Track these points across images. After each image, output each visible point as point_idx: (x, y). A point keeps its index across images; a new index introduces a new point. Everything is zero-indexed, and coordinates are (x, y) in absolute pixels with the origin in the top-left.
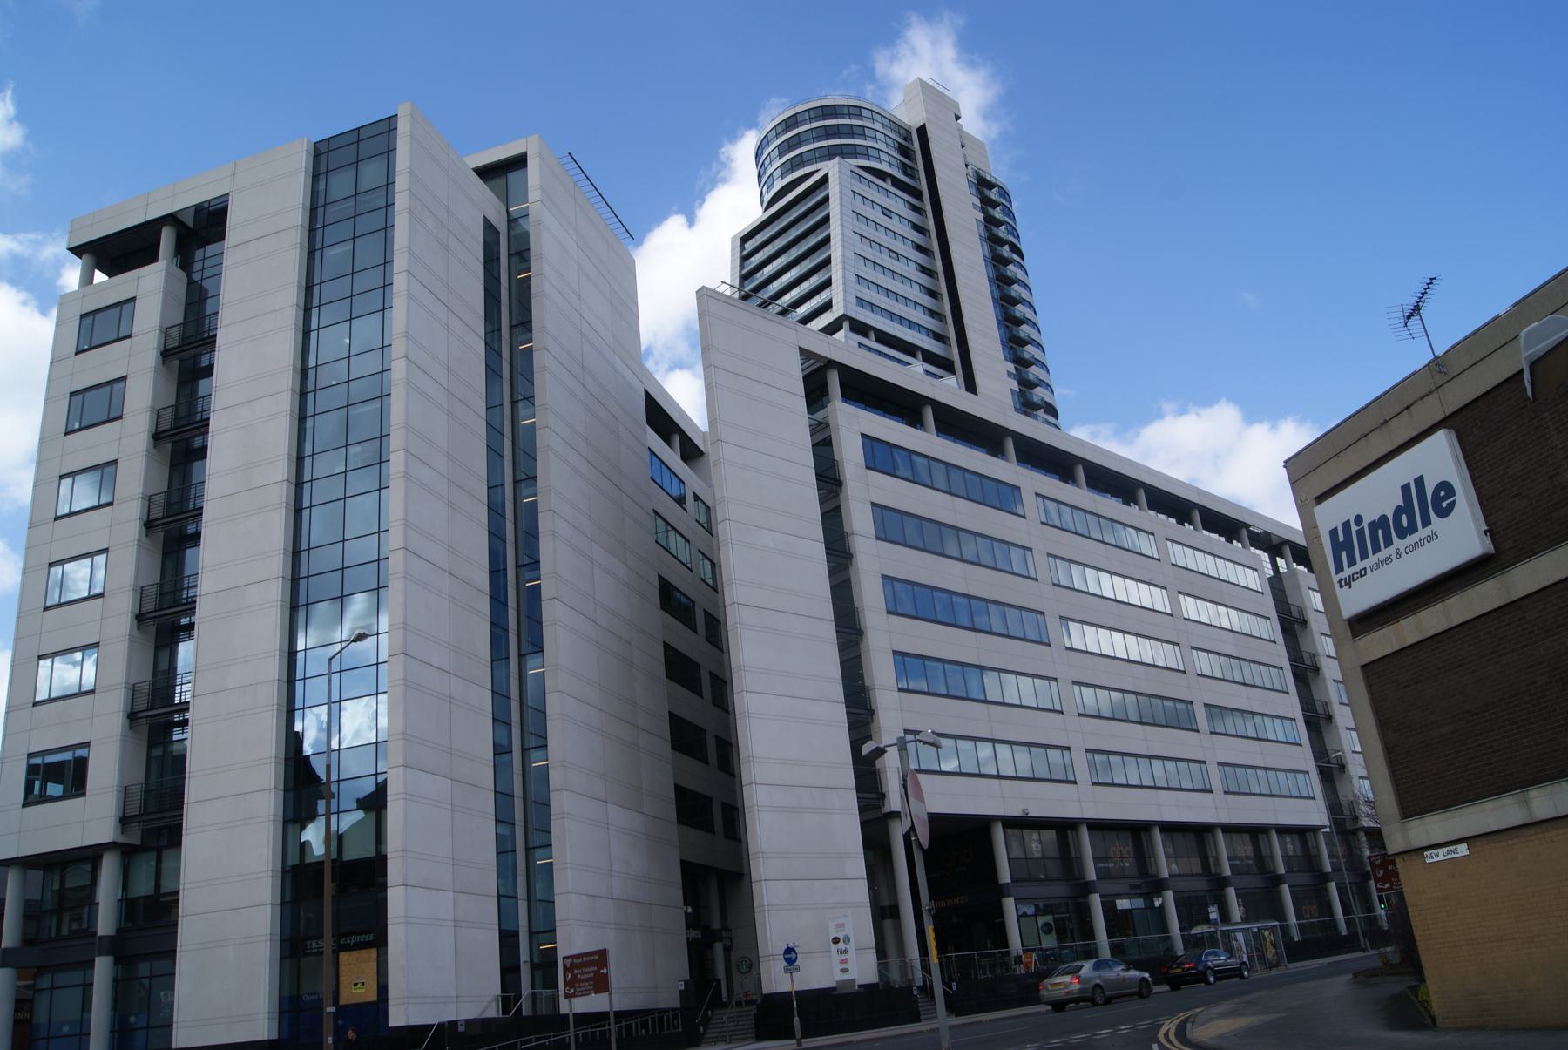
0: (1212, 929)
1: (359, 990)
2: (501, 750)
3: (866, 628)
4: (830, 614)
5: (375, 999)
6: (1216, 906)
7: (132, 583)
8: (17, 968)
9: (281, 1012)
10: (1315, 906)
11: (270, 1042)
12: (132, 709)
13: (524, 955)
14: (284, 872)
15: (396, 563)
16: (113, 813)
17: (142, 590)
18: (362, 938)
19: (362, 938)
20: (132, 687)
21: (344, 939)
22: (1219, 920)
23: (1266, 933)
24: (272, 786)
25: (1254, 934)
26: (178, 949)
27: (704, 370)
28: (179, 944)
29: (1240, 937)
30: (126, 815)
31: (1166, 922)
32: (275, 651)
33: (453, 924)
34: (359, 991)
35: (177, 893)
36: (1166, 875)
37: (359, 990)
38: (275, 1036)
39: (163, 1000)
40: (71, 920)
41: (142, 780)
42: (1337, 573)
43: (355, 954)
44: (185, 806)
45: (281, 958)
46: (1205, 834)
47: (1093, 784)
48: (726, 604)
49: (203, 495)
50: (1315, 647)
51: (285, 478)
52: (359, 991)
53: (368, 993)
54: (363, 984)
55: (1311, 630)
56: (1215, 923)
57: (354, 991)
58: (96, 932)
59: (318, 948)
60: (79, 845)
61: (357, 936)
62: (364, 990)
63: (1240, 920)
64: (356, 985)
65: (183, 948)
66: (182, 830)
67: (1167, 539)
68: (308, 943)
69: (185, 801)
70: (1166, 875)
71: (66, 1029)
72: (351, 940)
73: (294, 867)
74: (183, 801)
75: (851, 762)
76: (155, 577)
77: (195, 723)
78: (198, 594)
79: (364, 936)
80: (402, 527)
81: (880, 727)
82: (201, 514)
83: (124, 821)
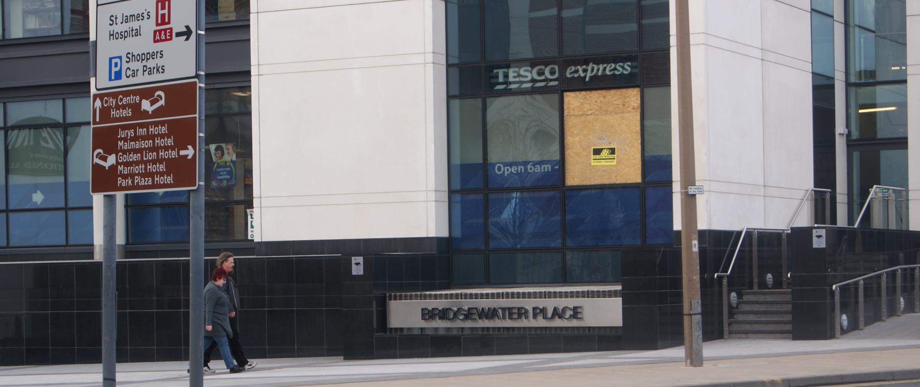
5: (638, 179)
11: (439, 240)
13: (840, 127)
18: (608, 69)
19: (608, 69)
21: (573, 68)
22: (388, 299)
31: (535, 285)
33: (758, 54)
38: (445, 233)
40: (26, 13)
42: (161, 10)
43: (595, 97)
45: (449, 97)
52: (603, 163)
54: (612, 151)
57: (594, 163)
58: (89, 39)
61: (598, 64)
62: (614, 163)
64: (597, 152)
65: (263, 70)
68: (501, 72)
71: (38, 198)
72: (585, 71)
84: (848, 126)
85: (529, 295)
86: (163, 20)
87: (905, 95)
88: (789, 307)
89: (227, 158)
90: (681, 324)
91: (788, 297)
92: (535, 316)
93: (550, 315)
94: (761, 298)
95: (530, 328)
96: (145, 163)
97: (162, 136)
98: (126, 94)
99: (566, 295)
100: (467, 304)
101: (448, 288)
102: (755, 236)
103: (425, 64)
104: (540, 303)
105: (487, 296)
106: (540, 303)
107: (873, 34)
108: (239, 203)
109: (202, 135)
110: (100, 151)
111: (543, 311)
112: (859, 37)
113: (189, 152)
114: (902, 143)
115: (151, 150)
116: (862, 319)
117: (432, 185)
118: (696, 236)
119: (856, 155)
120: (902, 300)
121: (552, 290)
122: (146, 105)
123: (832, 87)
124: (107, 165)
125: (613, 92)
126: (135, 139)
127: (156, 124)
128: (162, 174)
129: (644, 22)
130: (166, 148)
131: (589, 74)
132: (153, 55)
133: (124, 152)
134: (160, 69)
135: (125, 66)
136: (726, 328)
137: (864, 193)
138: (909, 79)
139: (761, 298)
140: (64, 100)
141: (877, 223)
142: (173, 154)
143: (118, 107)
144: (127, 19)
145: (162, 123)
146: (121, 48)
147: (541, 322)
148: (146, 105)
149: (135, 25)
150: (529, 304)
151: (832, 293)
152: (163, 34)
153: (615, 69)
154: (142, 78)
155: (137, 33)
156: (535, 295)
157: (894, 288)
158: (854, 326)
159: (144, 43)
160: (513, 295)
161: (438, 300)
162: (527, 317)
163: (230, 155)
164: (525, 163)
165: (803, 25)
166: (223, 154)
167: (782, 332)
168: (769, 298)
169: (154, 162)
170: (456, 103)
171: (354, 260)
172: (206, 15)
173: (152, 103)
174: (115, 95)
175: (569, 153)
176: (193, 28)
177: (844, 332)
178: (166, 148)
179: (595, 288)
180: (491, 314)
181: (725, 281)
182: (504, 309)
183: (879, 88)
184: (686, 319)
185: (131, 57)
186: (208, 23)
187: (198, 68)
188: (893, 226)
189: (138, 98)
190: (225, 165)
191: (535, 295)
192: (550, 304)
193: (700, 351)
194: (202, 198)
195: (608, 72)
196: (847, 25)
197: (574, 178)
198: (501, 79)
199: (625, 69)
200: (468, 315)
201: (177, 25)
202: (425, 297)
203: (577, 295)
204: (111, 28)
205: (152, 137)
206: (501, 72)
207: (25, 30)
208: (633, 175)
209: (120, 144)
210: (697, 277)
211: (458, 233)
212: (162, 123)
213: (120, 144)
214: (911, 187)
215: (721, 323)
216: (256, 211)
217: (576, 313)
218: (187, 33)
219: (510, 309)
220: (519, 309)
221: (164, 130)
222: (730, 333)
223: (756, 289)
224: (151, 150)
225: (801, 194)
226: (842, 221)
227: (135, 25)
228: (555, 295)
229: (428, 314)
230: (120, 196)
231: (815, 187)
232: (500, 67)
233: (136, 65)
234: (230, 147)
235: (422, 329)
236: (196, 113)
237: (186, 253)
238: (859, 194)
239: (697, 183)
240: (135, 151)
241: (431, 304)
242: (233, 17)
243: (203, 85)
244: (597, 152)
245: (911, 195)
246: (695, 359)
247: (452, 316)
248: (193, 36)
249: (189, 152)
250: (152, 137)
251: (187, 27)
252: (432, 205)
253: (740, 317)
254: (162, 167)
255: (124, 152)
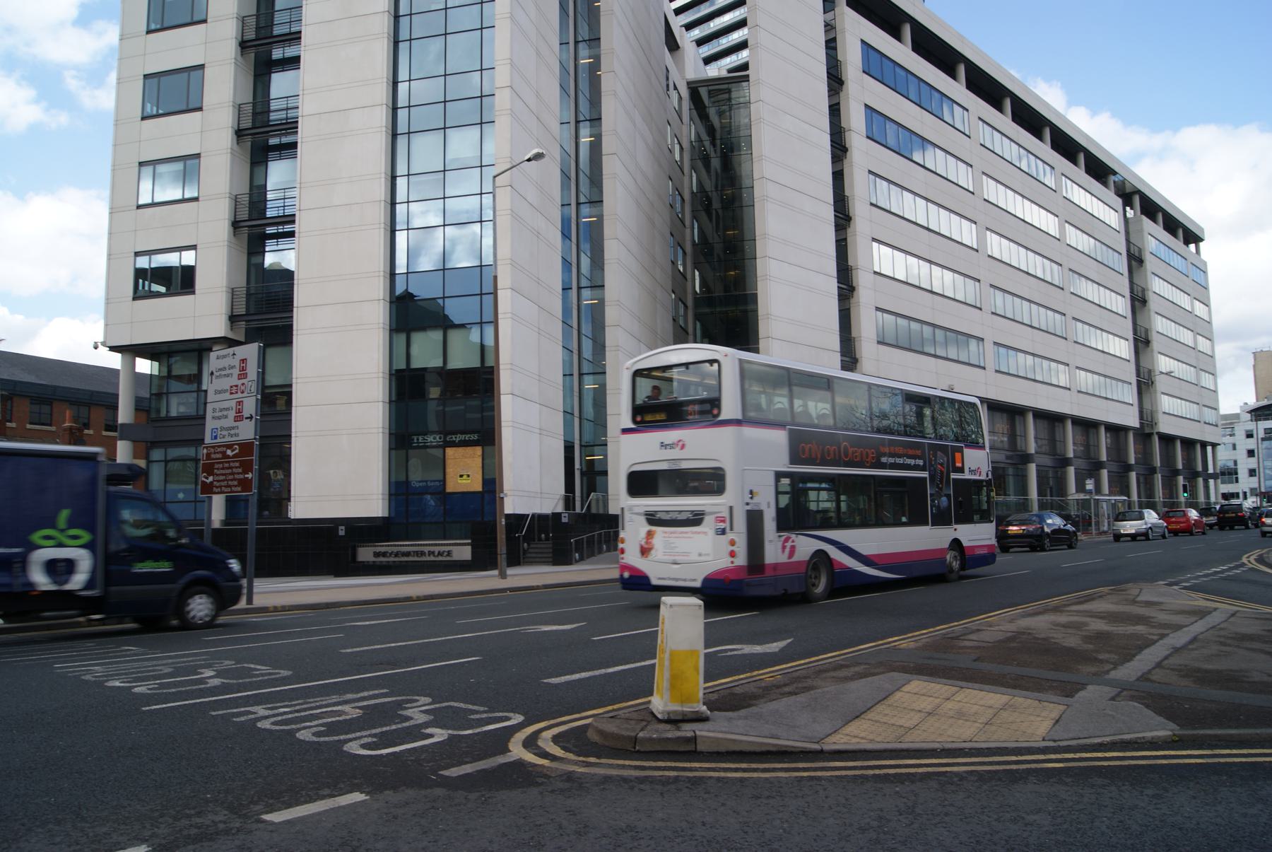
0: (1088, 497)
1: (464, 481)
2: (566, 289)
3: (855, 215)
4: (831, 201)
5: (481, 490)
6: (1093, 479)
7: (231, 100)
8: (134, 441)
9: (390, 495)
10: (1118, 489)
11: (383, 518)
12: (235, 218)
13: (577, 465)
14: (391, 375)
15: (502, 100)
16: (224, 311)
17: (240, 108)
18: (467, 437)
19: (467, 437)
20: (234, 198)
21: (450, 436)
23: (1120, 505)
24: (382, 298)
25: (1112, 504)
26: (293, 435)
27: (112, 212)
28: (293, 430)
29: (1104, 505)
30: (234, 314)
32: (381, 173)
33: (538, 431)
34: (464, 481)
35: (291, 386)
36: (1033, 451)
37: (464, 481)
38: (387, 515)
39: (272, 477)
40: (179, 404)
41: (244, 284)
43: (461, 450)
44: (295, 310)
45: (390, 449)
46: (1057, 424)
47: (997, 371)
48: (755, 178)
49: (301, 20)
50: (1146, 282)
51: (387, 10)
52: (464, 481)
53: (474, 483)
54: (468, 476)
55: (1146, 269)
56: (1090, 492)
57: (460, 482)
59: (425, 443)
60: (192, 338)
61: (462, 434)
62: (469, 481)
63: (1107, 493)
64: (461, 476)
66: (292, 330)
67: (1063, 174)
68: (415, 438)
69: (295, 305)
70: (1033, 451)
71: (181, 496)
72: (456, 438)
73: (398, 371)
74: (293, 305)
75: (838, 329)
76: (249, 98)
77: (301, 235)
78: (300, 114)
79: (469, 435)
80: (509, 66)
81: (859, 302)
82: (300, 38)
83: (233, 319)
84: (581, 465)
85: (426, 545)
86: (239, 411)
87: (606, 450)
88: (551, 550)
89: (279, 477)
90: (496, 558)
91: (551, 546)
92: (429, 555)
93: (436, 554)
94: (539, 546)
95: (427, 561)
96: (227, 480)
97: (237, 467)
98: (219, 446)
99: (444, 545)
100: (395, 549)
101: (388, 541)
102: (536, 516)
103: (378, 433)
104: (432, 549)
105: (406, 545)
106: (432, 549)
107: (592, 423)
108: (285, 499)
109: (257, 467)
110: (205, 474)
111: (433, 553)
112: (586, 425)
113: (250, 476)
114: (605, 473)
115: (230, 474)
116: (585, 555)
117: (380, 492)
118: (504, 517)
119: (585, 478)
120: (604, 546)
121: (437, 542)
122: (229, 452)
123: (573, 447)
124: (208, 481)
125: (469, 448)
126: (223, 469)
127: (234, 462)
128: (236, 486)
129: (484, 414)
130: (238, 473)
131: (458, 439)
132: (233, 428)
133: (217, 475)
134: (237, 435)
135: (219, 432)
136: (522, 561)
137: (588, 496)
138: (608, 444)
139: (539, 546)
140: (196, 447)
141: (594, 511)
142: (241, 476)
143: (215, 453)
144: (221, 410)
145: (237, 461)
146: (218, 424)
147: (432, 558)
148: (229, 452)
149: (225, 413)
150: (426, 549)
151: (571, 543)
152: (239, 417)
153: (452, 438)
154: (228, 439)
155: (226, 417)
156: (429, 545)
157: (601, 541)
158: (582, 559)
159: (229, 422)
160: (419, 545)
161: (383, 547)
162: (425, 556)
163: (280, 476)
164: (426, 481)
165: (560, 418)
166: (277, 475)
167: (548, 562)
168: (543, 546)
169: (232, 480)
170: (393, 452)
171: (340, 528)
172: (117, 396)
173: (232, 451)
174: (213, 447)
175: (448, 477)
176: (254, 415)
177: (577, 562)
178: (238, 473)
179: (458, 542)
180: (407, 554)
181: (521, 538)
182: (414, 552)
183: (596, 448)
184: (499, 556)
185: (222, 429)
186: (264, 414)
187: (256, 434)
188: (601, 511)
189: (225, 449)
190: (278, 480)
191: (429, 545)
192: (436, 549)
193: (506, 572)
194: (256, 497)
195: (467, 439)
196: (580, 418)
197: (450, 488)
198: (415, 441)
199: (475, 437)
200: (397, 555)
201: (246, 414)
202: (375, 546)
203: (450, 545)
204: (213, 414)
205: (231, 468)
206: (415, 438)
207: (178, 413)
208: (478, 487)
209: (215, 471)
210: (504, 536)
211: (393, 515)
212: (237, 461)
213: (215, 471)
214: (610, 493)
215: (519, 557)
216: (292, 503)
217: (449, 553)
218: (251, 418)
219: (417, 552)
220: (422, 551)
221: (237, 464)
222: (523, 562)
223: (536, 542)
224: (230, 474)
225: (558, 497)
226: (578, 510)
227: (225, 413)
228: (439, 545)
229: (377, 555)
230: (925, 474)
231: (566, 493)
232: (416, 435)
233: (225, 433)
234: (281, 472)
235: (374, 562)
236: (253, 456)
237: (246, 524)
238: (585, 498)
239: (505, 492)
240: (223, 475)
241: (379, 549)
242: (284, 408)
243: (258, 443)
244: (461, 476)
245: (610, 497)
246: (503, 576)
247: (388, 555)
248: (254, 420)
249: (250, 476)
250: (231, 468)
251: (251, 415)
252: (381, 501)
253: (529, 555)
254: (236, 483)
255: (217, 475)
